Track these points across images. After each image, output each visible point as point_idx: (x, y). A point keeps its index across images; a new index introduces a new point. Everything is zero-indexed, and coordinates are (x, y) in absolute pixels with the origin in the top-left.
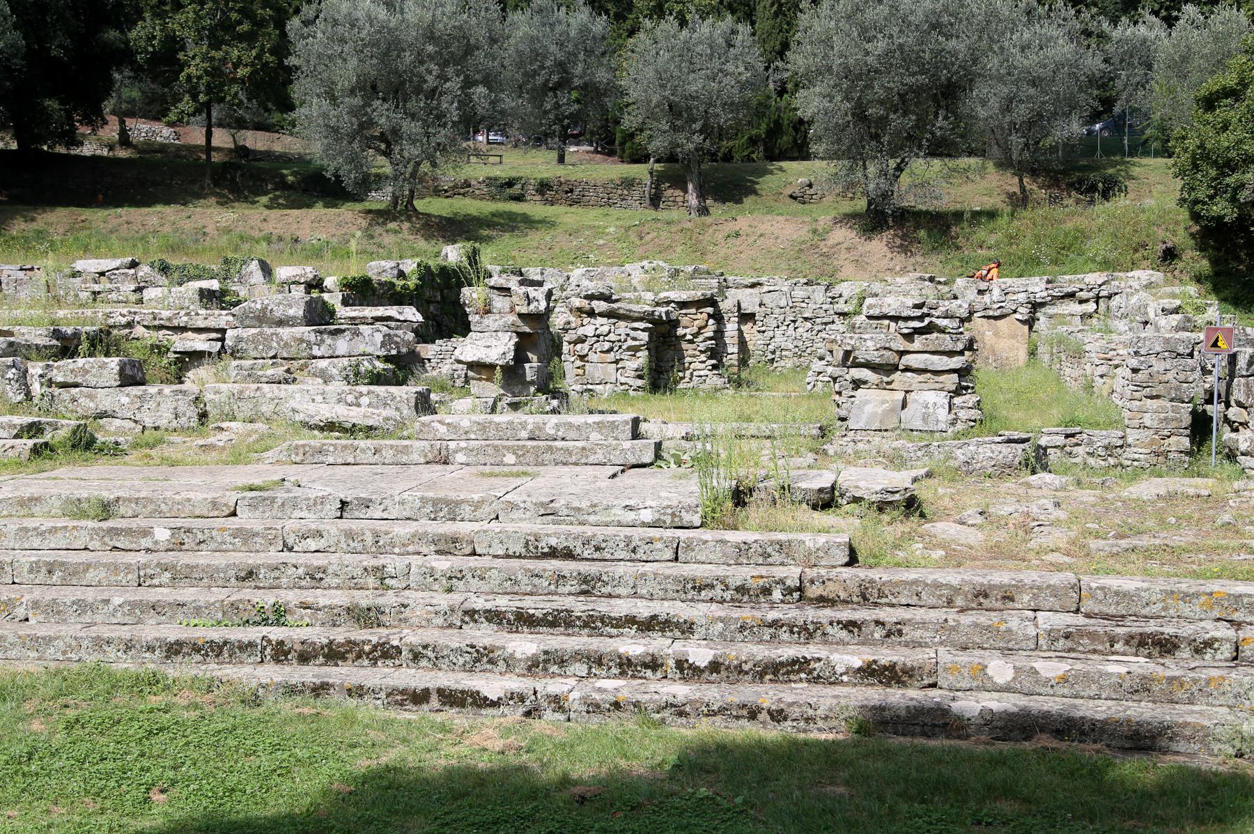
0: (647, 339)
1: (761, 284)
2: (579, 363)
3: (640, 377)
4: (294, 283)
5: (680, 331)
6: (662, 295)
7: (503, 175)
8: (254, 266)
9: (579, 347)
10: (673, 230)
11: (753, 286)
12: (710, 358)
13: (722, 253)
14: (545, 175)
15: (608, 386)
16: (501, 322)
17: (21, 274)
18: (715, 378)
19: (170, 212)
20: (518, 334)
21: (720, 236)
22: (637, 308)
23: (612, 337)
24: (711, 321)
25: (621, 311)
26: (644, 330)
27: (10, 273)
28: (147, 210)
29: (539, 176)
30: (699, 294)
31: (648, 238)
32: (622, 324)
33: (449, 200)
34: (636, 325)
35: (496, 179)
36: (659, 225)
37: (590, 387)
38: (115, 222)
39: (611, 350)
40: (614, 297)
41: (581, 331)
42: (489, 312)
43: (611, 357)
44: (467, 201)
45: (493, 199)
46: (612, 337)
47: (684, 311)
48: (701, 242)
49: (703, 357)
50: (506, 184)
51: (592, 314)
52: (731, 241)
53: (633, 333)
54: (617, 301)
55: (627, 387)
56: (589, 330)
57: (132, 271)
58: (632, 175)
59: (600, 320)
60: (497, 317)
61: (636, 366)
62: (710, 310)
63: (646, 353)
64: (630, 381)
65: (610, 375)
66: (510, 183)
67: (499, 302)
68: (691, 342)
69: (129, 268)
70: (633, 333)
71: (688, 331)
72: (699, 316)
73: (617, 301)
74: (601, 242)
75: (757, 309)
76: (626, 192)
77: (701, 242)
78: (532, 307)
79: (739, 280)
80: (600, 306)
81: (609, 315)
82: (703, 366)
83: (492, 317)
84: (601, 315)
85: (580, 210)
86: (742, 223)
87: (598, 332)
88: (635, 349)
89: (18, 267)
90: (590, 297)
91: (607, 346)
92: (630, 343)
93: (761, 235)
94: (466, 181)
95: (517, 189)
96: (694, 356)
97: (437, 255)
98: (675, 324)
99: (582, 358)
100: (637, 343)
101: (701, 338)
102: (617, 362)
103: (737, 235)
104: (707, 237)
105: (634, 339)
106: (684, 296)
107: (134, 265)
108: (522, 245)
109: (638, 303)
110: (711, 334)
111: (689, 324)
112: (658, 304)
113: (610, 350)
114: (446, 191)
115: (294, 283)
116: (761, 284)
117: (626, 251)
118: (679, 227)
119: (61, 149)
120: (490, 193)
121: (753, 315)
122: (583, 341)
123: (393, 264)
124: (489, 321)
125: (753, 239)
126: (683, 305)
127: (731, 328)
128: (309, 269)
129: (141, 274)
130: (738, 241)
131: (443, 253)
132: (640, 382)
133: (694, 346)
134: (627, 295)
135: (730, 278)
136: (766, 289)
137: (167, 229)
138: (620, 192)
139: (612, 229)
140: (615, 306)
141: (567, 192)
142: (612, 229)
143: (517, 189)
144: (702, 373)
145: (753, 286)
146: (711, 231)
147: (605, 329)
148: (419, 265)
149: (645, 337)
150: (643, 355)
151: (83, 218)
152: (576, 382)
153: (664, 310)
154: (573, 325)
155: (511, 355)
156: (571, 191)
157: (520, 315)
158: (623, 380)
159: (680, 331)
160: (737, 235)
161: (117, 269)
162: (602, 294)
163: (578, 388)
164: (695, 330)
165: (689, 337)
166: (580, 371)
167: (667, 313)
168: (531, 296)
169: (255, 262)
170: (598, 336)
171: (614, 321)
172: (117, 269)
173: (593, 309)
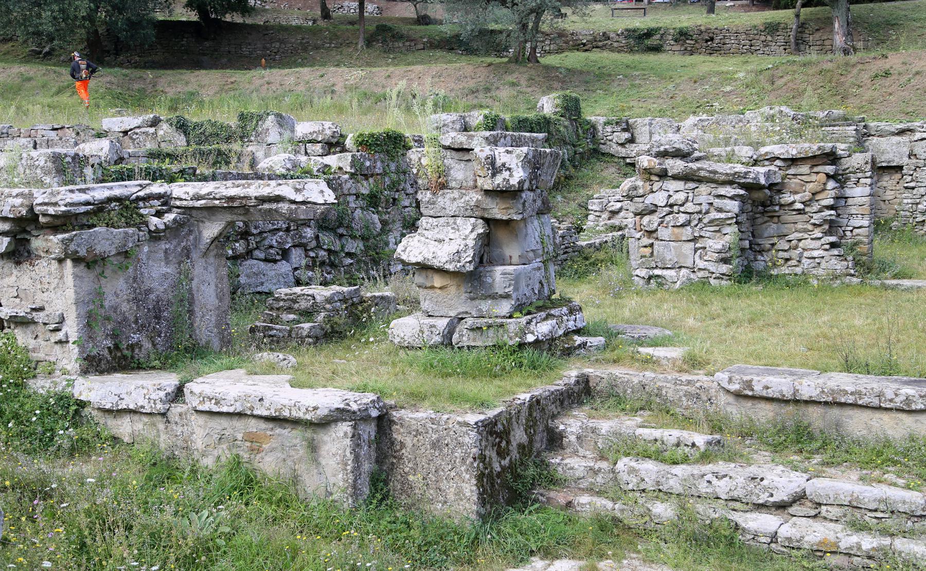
0: (736, 210)
1: (911, 131)
2: (646, 241)
3: (725, 261)
4: (310, 142)
5: (787, 198)
6: (763, 150)
7: (642, 26)
8: (270, 121)
9: (646, 219)
10: (810, 72)
11: (901, 132)
12: (826, 233)
13: (868, 95)
14: (685, 24)
15: (683, 271)
16: (461, 203)
17: (54, 133)
18: (834, 261)
19: (305, 72)
20: (487, 221)
21: (865, 77)
22: (724, 168)
23: (689, 207)
24: (831, 184)
25: (702, 173)
26: (732, 198)
27: (44, 132)
28: (287, 71)
29: (679, 25)
30: (815, 147)
31: (780, 82)
32: (704, 189)
33: (587, 54)
34: (722, 191)
35: (634, 31)
36: (795, 68)
37: (657, 272)
38: (258, 82)
39: (687, 224)
40: (697, 154)
41: (649, 200)
42: (443, 186)
43: (687, 232)
44: (605, 54)
45: (631, 51)
46: (689, 207)
47: (792, 171)
48: (842, 84)
49: (817, 233)
50: (644, 34)
51: (663, 175)
52: (879, 81)
53: (718, 202)
54: (698, 159)
55: (707, 274)
56: (660, 198)
57: (152, 130)
58: (777, 20)
59: (673, 185)
60: (456, 194)
61: (719, 247)
62: (830, 169)
63: (735, 228)
64: (712, 267)
65: (686, 256)
66: (649, 34)
67: (459, 172)
68: (800, 212)
69: (151, 126)
70: (718, 202)
71: (797, 197)
72: (814, 177)
73: (698, 159)
74: (728, 88)
75: (905, 160)
76: (769, 38)
77: (842, 84)
78: (499, 180)
79: (883, 125)
80: (676, 165)
81: (686, 177)
82: (817, 244)
83: (450, 194)
84: (675, 177)
85: (720, 59)
86: (894, 61)
87: (671, 201)
88: (719, 224)
89: (49, 126)
90: (664, 154)
91: (682, 218)
92: (714, 215)
93: (917, 73)
94: (604, 34)
95: (654, 41)
96: (806, 231)
97: (534, 107)
98: (776, 188)
99: (650, 233)
100: (723, 215)
101: (815, 207)
102: (694, 240)
103: (887, 74)
104: (849, 80)
105: (720, 210)
106: (793, 151)
107: (155, 123)
108: (643, 95)
109: (729, 160)
110: (830, 202)
111: (803, 186)
112: (756, 163)
113: (687, 224)
114: (584, 45)
115: (310, 142)
116: (911, 131)
117: (755, 97)
118: (818, 69)
119: (238, 19)
120: (628, 45)
121: (899, 168)
122: (652, 212)
123: (454, 116)
124: (447, 201)
125: (906, 77)
126: (793, 161)
127: (859, 193)
128: (328, 124)
129: (161, 133)
130: (887, 82)
131: (539, 105)
132: (724, 268)
133: (805, 217)
134: (716, 150)
135: (872, 124)
136: (918, 136)
137: (301, 88)
138: (763, 38)
139: (741, 75)
140: (694, 166)
141: (707, 41)
142: (741, 75)
143: (654, 41)
144: (815, 253)
145: (901, 132)
146: (855, 71)
147: (681, 197)
148: (486, 117)
149: (734, 206)
150: (731, 231)
151: (233, 80)
152: (640, 266)
153: (762, 170)
154: (641, 191)
155: (468, 256)
156: (712, 39)
157: (487, 192)
158: (701, 264)
159: (787, 198)
160: (887, 74)
161: (139, 127)
162: (678, 150)
163: (643, 273)
164: (807, 195)
165: (799, 206)
166: (649, 250)
167: (768, 175)
168: (499, 163)
169: (271, 118)
170: (671, 206)
171: (691, 185)
172: (139, 127)
173: (666, 170)
